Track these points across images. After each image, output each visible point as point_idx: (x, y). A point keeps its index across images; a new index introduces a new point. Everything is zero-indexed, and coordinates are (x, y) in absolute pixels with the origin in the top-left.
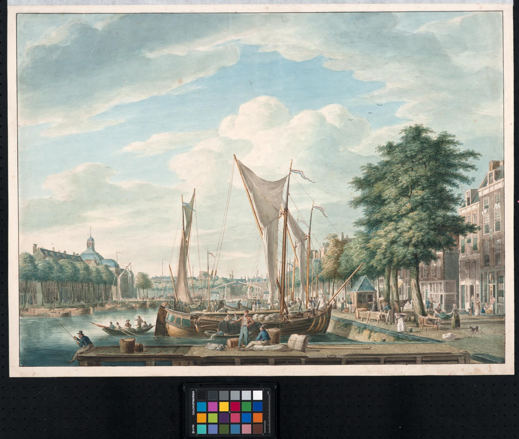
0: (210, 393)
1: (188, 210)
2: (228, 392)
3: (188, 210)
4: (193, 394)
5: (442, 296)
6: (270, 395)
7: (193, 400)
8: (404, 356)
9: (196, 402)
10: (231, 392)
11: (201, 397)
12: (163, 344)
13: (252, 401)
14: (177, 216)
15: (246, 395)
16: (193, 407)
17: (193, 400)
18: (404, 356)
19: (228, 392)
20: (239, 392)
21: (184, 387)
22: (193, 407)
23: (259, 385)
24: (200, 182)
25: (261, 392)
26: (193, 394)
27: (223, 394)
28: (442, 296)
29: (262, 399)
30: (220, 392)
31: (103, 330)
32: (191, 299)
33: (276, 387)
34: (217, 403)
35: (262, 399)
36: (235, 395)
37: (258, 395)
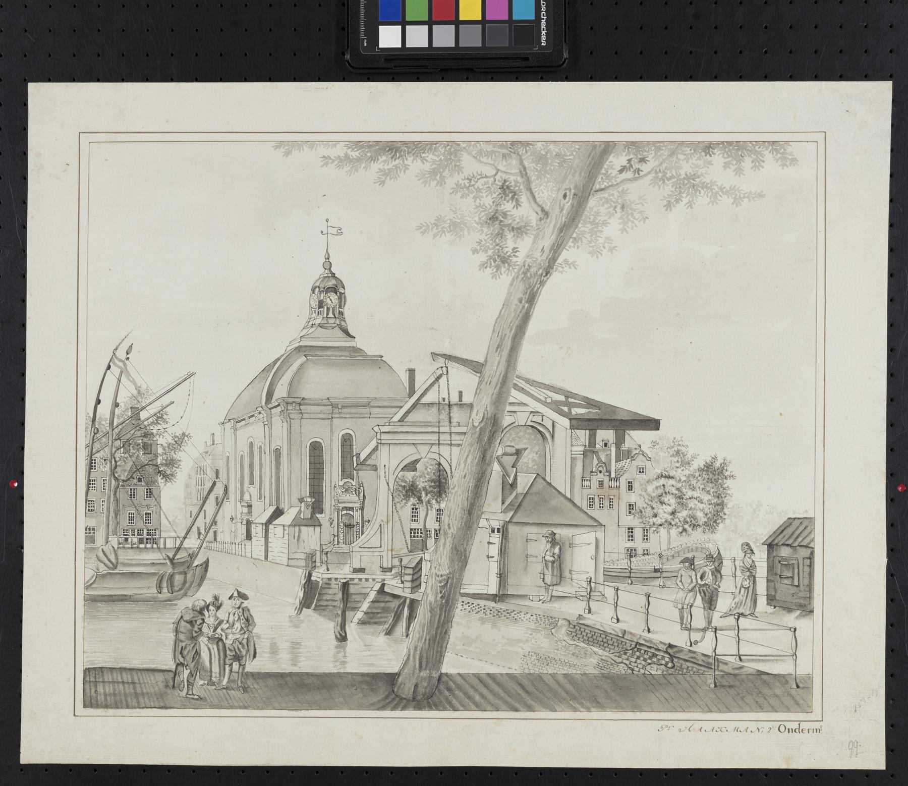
0: (502, 42)
1: (266, 558)
2: (461, 45)
4: (543, 38)
5: (316, 449)
6: (362, 36)
7: (543, 24)
10: (400, 46)
11: (527, 30)
13: (404, 23)
14: (183, 374)
15: (418, 38)
16: (544, 8)
17: (543, 24)
19: (461, 45)
20: (409, 45)
22: (544, 8)
23: (386, 60)
25: (382, 45)
26: (543, 38)
27: (472, 39)
28: (316, 449)
29: (381, 28)
31: (339, 167)
33: (347, 57)
34: (426, 19)
35: (381, 28)
36: (445, 37)
37: (389, 37)
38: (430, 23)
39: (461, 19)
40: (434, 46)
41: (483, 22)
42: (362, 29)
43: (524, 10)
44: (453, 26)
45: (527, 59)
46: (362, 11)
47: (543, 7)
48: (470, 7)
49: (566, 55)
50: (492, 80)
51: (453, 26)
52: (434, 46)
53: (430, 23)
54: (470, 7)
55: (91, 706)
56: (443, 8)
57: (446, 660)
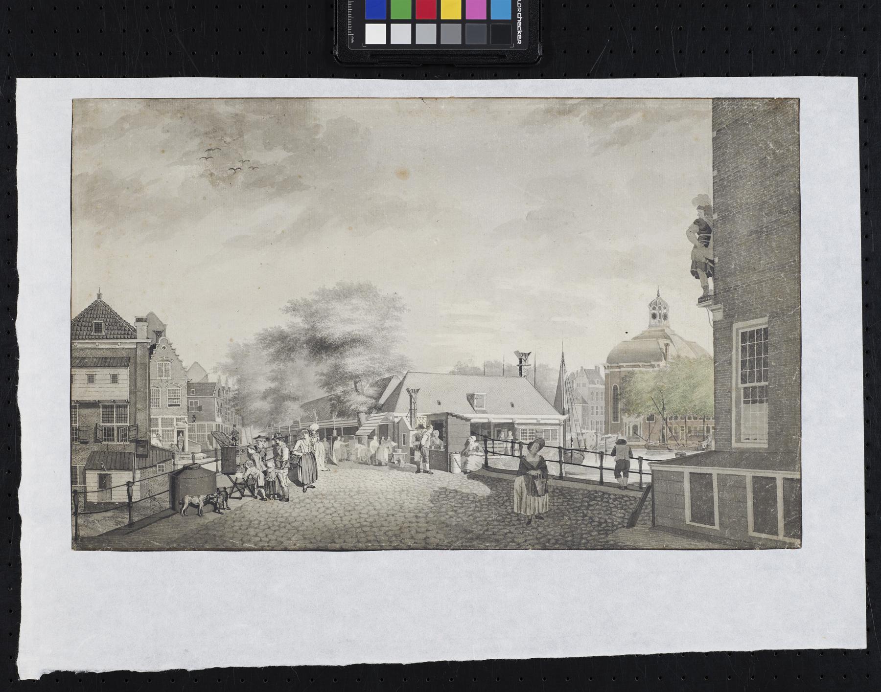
0: (480, 39)
1: (521, 374)
3: (521, 374)
4: (519, 37)
6: (349, 33)
8: (501, 476)
9: (515, 19)
10: (410, 43)
11: (501, 30)
12: (570, 474)
13: (389, 22)
15: (401, 35)
16: (519, 9)
18: (501, 476)
20: (418, 42)
21: (540, 53)
22: (519, 9)
23: (371, 55)
24: (231, 340)
26: (519, 37)
27: (453, 37)
30: (460, 43)
32: (561, 473)
36: (427, 35)
37: (375, 34)
38: (413, 22)
39: (442, 18)
40: (392, 43)
41: (463, 21)
42: (350, 26)
43: (501, 11)
44: (435, 25)
45: (504, 56)
46: (350, 10)
47: (519, 8)
48: (451, 7)
49: (540, 53)
50: (356, 77)
51: (435, 25)
52: (392, 43)
53: (413, 22)
54: (451, 7)
55: (771, 478)
56: (426, 8)
57: (766, 419)
